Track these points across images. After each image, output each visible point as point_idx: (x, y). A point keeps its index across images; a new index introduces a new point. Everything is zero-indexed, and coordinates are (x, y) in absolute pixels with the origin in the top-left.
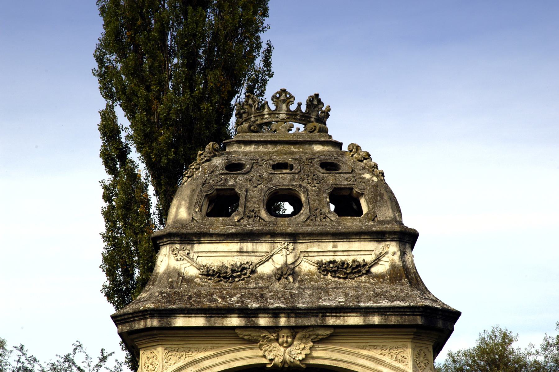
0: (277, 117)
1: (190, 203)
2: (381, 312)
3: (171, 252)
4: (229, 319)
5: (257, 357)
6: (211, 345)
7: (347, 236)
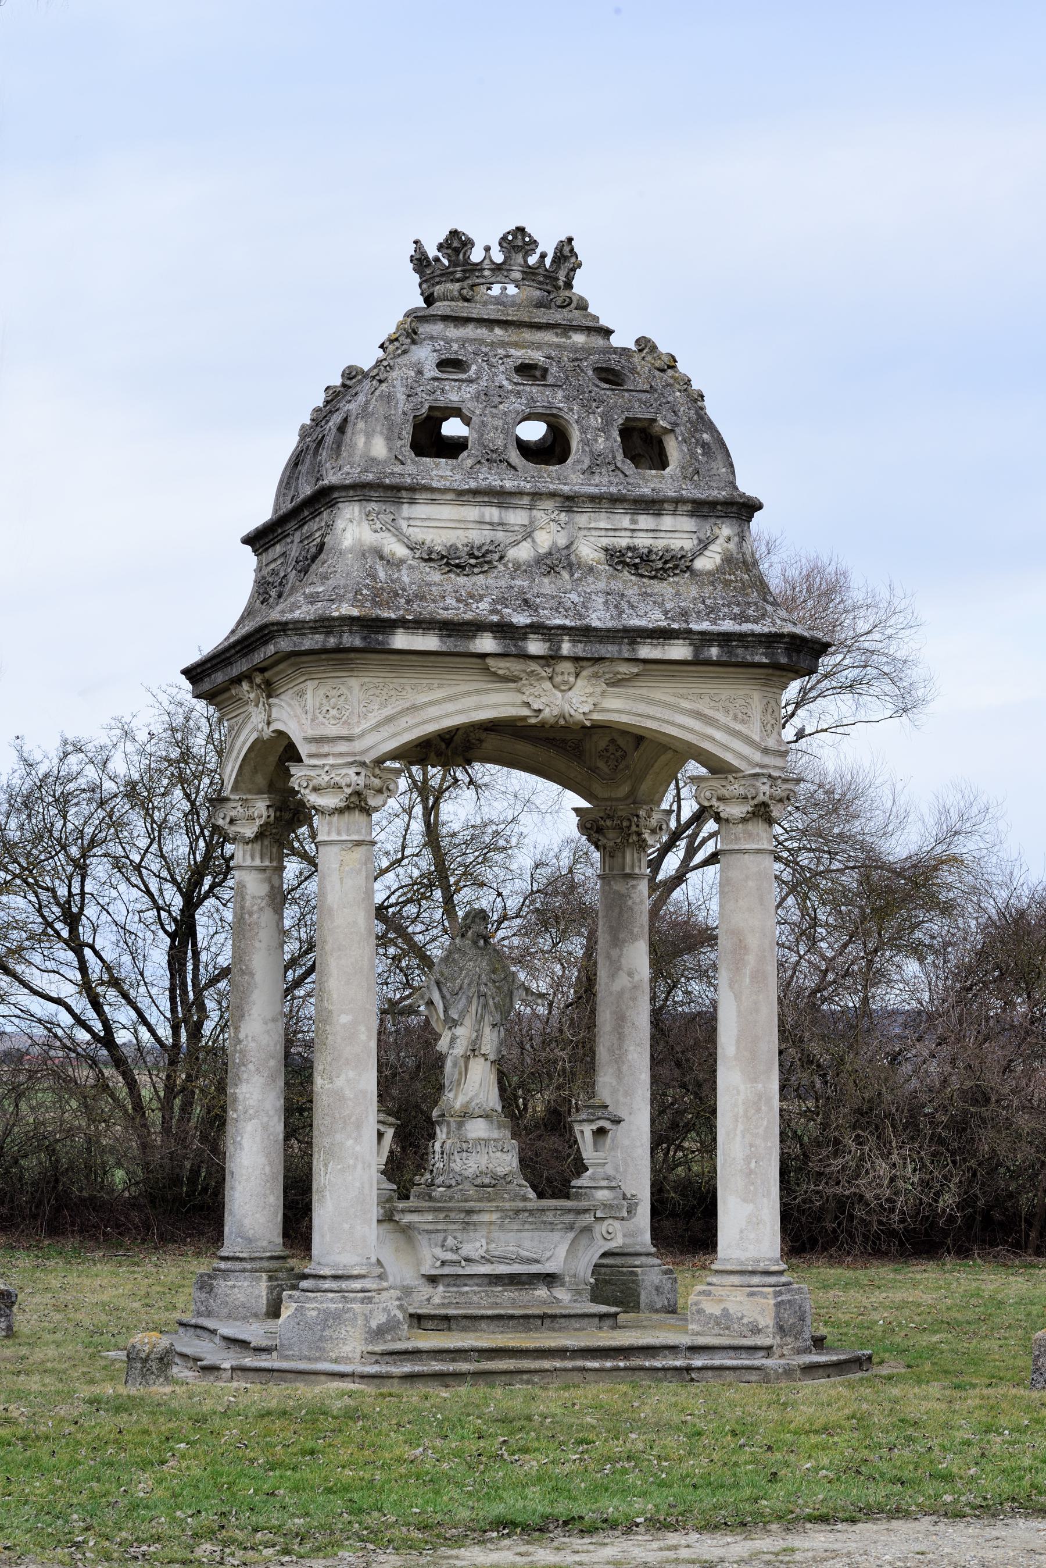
3: (364, 517)
4: (478, 641)
5: (513, 705)
6: (438, 681)
7: (653, 506)
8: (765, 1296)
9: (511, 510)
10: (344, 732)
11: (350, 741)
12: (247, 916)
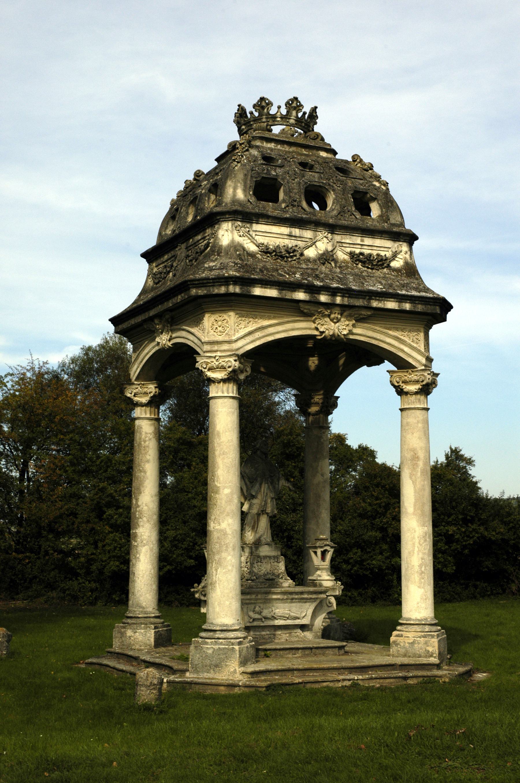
0: (288, 122)
1: (245, 186)
2: (412, 300)
4: (296, 293)
5: (310, 329)
6: (273, 315)
8: (433, 637)
9: (304, 230)
10: (227, 339)
11: (230, 343)
12: (143, 443)
